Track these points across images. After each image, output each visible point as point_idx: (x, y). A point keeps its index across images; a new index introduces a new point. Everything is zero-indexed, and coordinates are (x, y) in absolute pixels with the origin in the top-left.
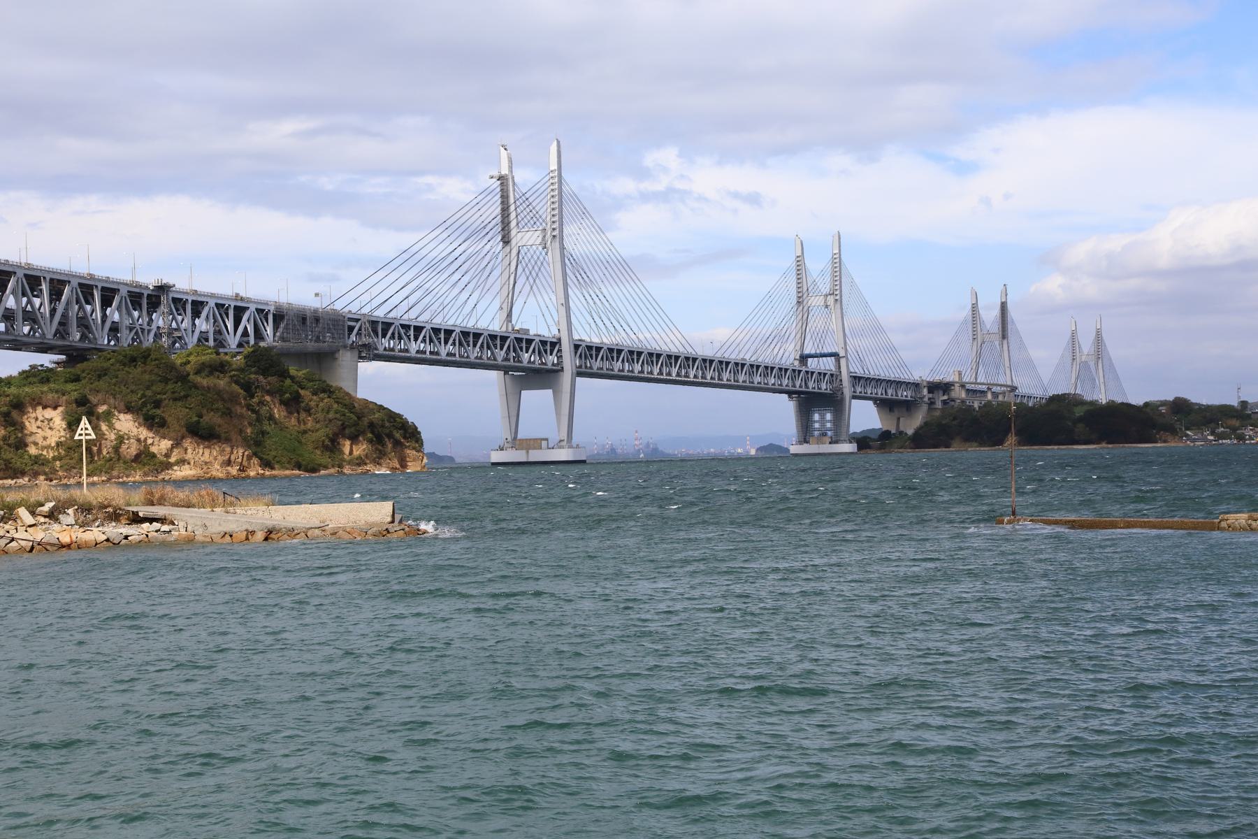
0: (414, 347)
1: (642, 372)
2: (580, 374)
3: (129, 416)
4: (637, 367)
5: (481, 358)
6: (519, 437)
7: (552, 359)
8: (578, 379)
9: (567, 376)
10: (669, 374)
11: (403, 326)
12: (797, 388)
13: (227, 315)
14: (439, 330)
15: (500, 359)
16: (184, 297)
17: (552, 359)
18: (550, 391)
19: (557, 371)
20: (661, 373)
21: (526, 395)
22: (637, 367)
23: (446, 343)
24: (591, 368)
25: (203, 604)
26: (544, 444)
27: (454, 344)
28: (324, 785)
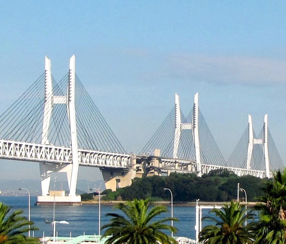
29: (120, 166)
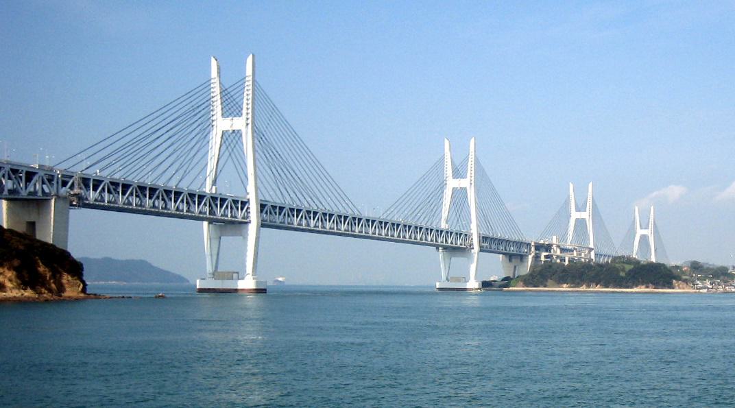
0: (296, 221)
1: (387, 235)
4: (384, 232)
5: (284, 223)
6: (219, 270)
7: (240, 215)
8: (263, 230)
9: (252, 228)
12: (449, 244)
13: (21, 179)
14: (276, 207)
15: (295, 223)
16: (20, 169)
17: (240, 215)
19: (244, 223)
20: (399, 236)
22: (384, 232)
23: (199, 204)
24: (354, 231)
25: (367, 381)
26: (235, 275)
29: (352, 231)
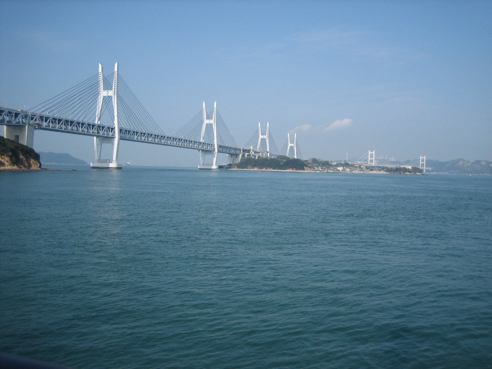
2: (121, 139)
3: (9, 158)
5: (130, 138)
6: (101, 159)
7: (111, 134)
8: (121, 141)
10: (184, 145)
11: (53, 119)
13: (13, 116)
14: (127, 131)
17: (111, 134)
18: (111, 144)
20: (182, 145)
21: (206, 155)
23: (92, 129)
26: (108, 161)
27: (123, 133)
28: (437, 221)
